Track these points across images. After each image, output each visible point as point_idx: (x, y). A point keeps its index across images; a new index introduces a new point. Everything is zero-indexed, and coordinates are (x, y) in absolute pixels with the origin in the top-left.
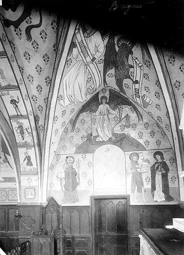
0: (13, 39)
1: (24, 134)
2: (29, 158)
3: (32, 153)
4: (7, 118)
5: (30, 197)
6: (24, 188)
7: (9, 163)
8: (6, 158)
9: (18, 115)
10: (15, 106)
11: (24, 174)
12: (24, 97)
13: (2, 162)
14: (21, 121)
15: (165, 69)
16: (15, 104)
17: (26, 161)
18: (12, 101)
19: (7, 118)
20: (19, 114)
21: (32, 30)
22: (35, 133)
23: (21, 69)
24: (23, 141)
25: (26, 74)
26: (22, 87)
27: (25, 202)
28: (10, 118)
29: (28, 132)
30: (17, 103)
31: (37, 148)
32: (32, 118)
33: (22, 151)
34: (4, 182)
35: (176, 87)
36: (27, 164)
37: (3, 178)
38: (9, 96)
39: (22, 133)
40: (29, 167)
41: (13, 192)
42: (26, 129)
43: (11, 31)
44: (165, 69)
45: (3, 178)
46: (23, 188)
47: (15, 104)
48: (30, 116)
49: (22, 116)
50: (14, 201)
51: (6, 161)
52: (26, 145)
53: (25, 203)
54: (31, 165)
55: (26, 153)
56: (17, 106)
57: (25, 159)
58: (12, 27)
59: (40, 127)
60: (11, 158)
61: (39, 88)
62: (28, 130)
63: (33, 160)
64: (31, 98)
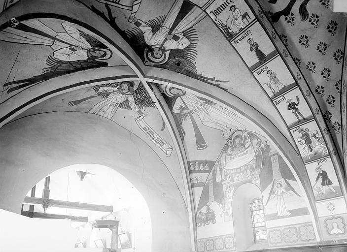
0: (284, 30)
1: (310, 142)
2: (324, 175)
3: (328, 166)
4: (285, 131)
5: (336, 231)
6: (324, 219)
7: (293, 190)
8: (289, 185)
9: (299, 121)
10: (294, 110)
11: (319, 198)
12: (305, 93)
13: (284, 191)
14: (304, 127)
15: (191, 193)
16: (295, 108)
17: (321, 179)
18: (289, 106)
19: (285, 131)
20: (301, 118)
21: (116, 22)
22: (327, 137)
23: (297, 61)
24: (311, 153)
25: (304, 63)
26: (302, 82)
27: (330, 240)
28: (289, 129)
29: (316, 138)
30: (297, 105)
31: (334, 157)
32: (320, 117)
33: (312, 169)
34: (291, 216)
35: (310, 70)
36: (323, 184)
37: (290, 211)
38: (286, 101)
39: (308, 142)
40: (327, 187)
41: (306, 229)
42: (314, 135)
43: (281, 25)
44: (191, 193)
45: (290, 211)
46: (322, 220)
47: (295, 108)
48: (317, 116)
49: (306, 120)
50: (310, 242)
51: (289, 187)
52: (317, 157)
53: (329, 242)
54: (330, 183)
55: (319, 168)
56: (297, 109)
57: (318, 178)
58: (282, 18)
59: (334, 127)
60: (297, 184)
61: (326, 73)
62: (317, 136)
63: (332, 176)
64: (314, 91)
